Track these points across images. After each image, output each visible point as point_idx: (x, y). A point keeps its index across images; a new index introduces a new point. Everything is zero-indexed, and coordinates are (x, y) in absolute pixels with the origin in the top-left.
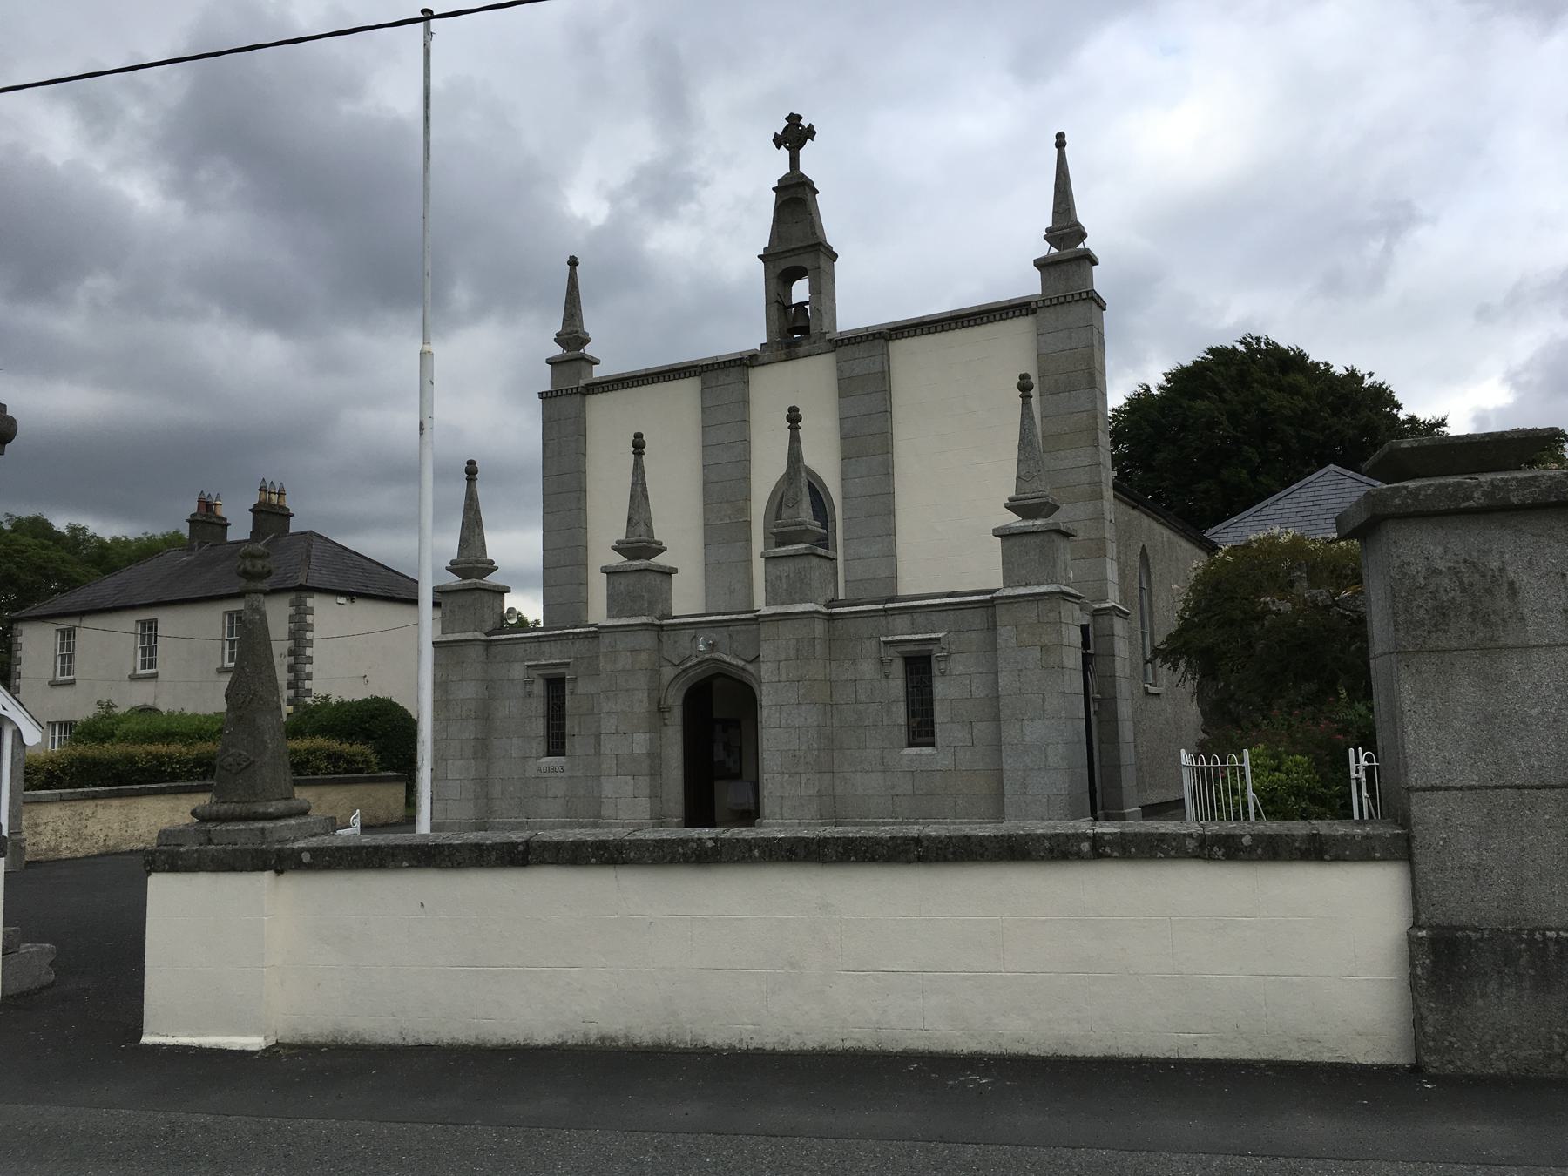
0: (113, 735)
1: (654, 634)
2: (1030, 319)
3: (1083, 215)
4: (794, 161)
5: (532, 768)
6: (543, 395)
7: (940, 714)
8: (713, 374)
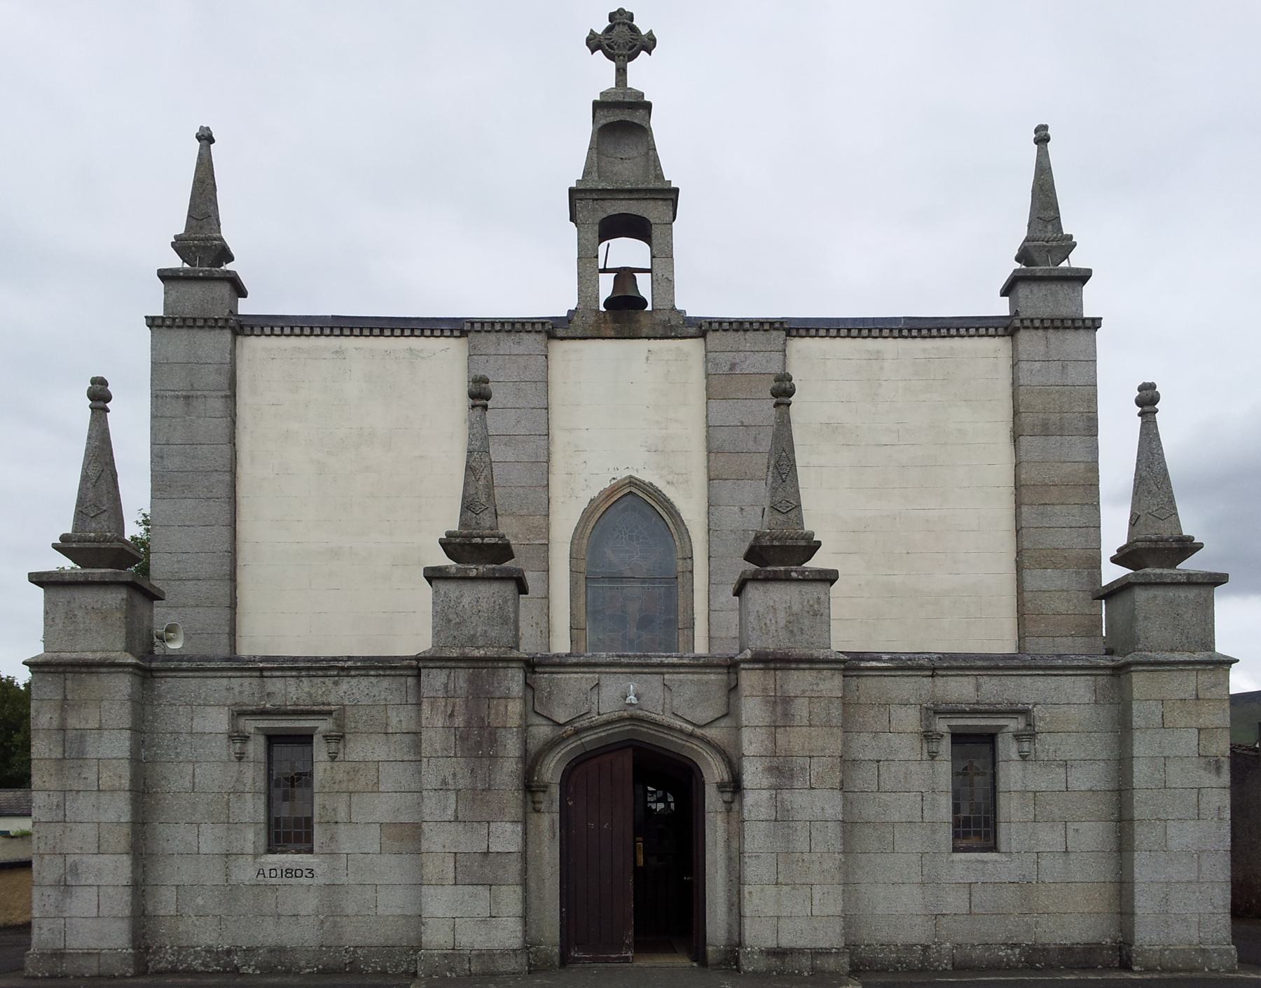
0: (532, 792)
1: (165, 685)
2: (463, 340)
3: (231, 233)
4: (621, 73)
5: (245, 872)
6: (152, 322)
7: (1010, 809)
8: (492, 337)
